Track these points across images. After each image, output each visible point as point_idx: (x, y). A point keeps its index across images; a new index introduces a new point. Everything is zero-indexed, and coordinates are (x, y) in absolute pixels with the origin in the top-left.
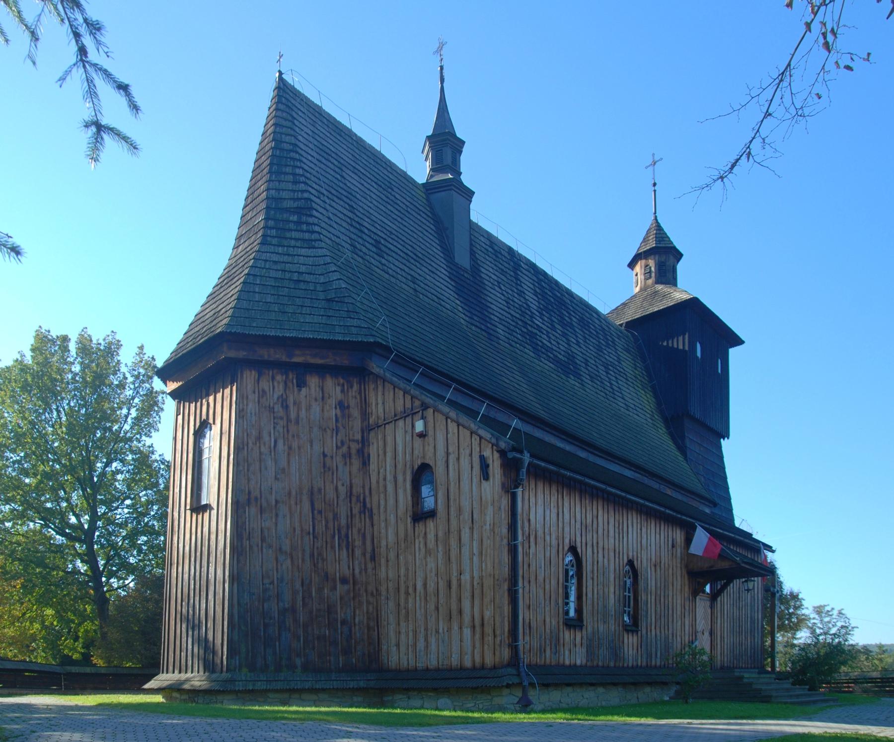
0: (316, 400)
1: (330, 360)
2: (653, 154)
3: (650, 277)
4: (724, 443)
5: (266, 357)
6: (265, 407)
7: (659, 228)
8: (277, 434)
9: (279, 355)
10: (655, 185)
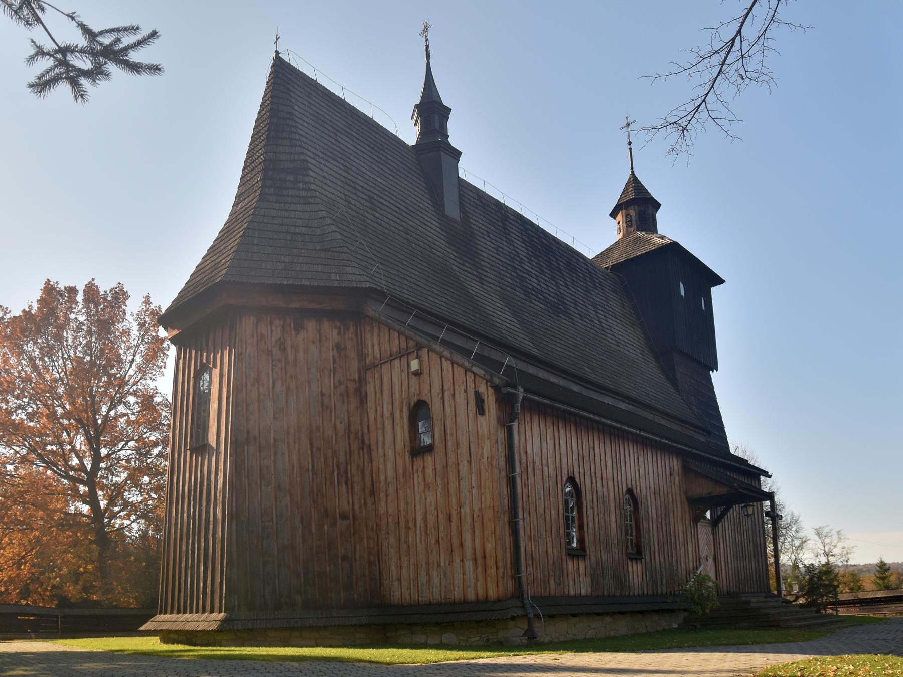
2: (627, 118)
4: (714, 375)
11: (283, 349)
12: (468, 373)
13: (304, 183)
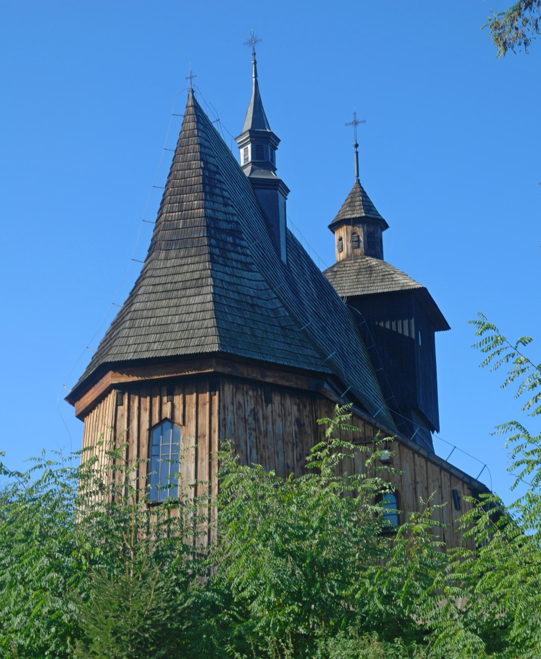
0: (279, 416)
1: (292, 383)
2: (355, 114)
3: (359, 247)
4: (434, 436)
5: (245, 375)
6: (242, 419)
7: (196, 107)
8: (251, 443)
9: (255, 375)
10: (357, 146)
11: (256, 420)
12: (443, 473)
13: (242, 247)
